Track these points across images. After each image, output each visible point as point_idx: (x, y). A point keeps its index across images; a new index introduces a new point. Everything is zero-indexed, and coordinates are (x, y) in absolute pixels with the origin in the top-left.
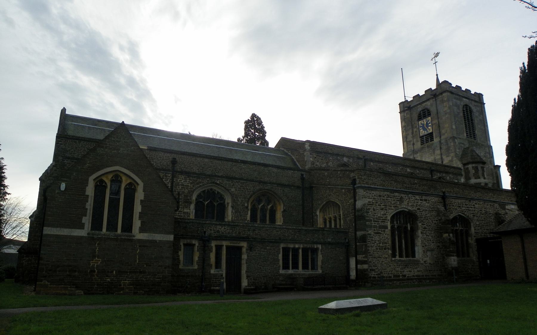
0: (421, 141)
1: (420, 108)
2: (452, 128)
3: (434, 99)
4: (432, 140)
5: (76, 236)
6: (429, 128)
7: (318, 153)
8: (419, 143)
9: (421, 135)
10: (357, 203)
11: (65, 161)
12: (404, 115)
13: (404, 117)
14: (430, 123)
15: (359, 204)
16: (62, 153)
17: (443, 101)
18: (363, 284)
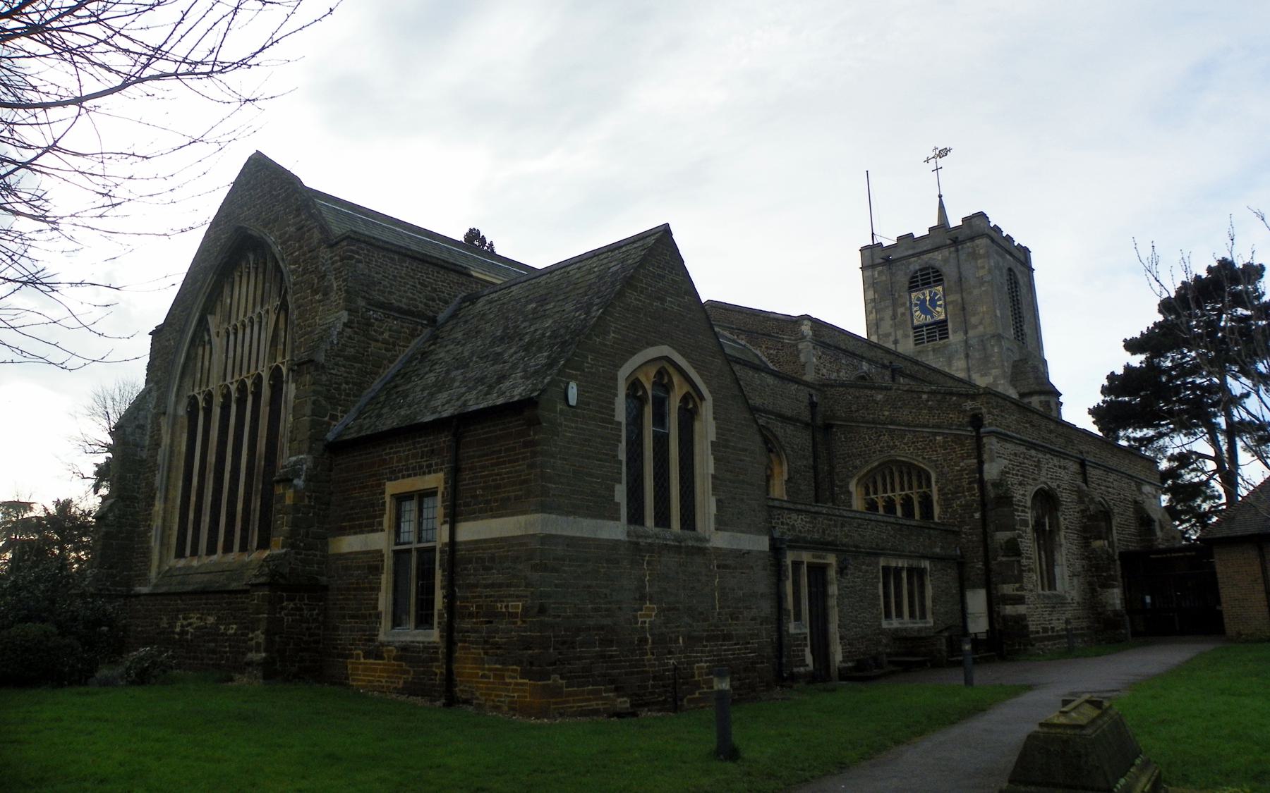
0: (915, 337)
1: (915, 265)
2: (996, 316)
3: (952, 249)
4: (944, 334)
5: (608, 540)
6: (938, 309)
7: (825, 346)
8: (911, 340)
9: (916, 323)
10: (986, 466)
11: (371, 312)
12: (873, 275)
13: (874, 279)
14: (939, 299)
15: (992, 471)
16: (365, 289)
17: (974, 255)
18: (1022, 647)
